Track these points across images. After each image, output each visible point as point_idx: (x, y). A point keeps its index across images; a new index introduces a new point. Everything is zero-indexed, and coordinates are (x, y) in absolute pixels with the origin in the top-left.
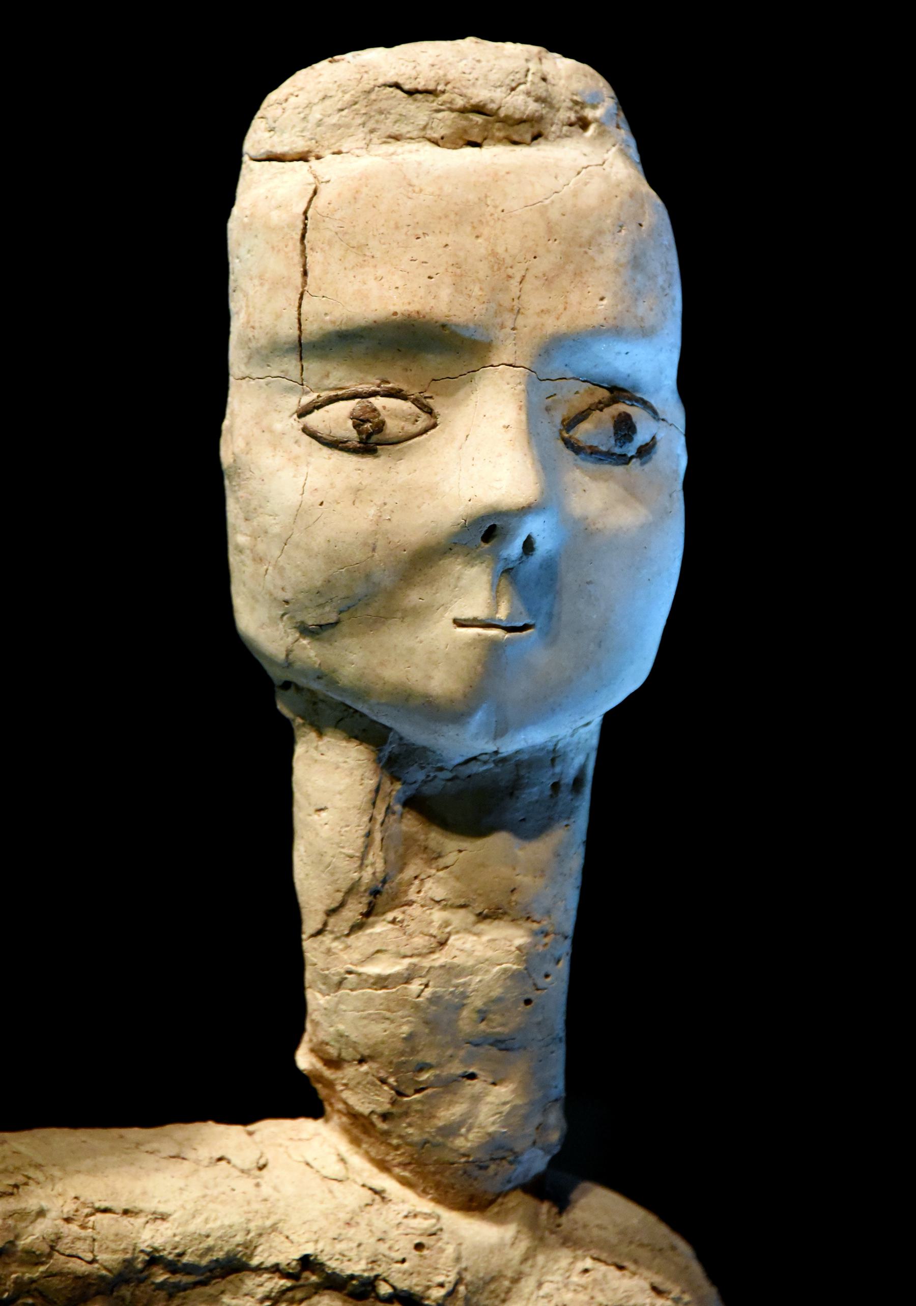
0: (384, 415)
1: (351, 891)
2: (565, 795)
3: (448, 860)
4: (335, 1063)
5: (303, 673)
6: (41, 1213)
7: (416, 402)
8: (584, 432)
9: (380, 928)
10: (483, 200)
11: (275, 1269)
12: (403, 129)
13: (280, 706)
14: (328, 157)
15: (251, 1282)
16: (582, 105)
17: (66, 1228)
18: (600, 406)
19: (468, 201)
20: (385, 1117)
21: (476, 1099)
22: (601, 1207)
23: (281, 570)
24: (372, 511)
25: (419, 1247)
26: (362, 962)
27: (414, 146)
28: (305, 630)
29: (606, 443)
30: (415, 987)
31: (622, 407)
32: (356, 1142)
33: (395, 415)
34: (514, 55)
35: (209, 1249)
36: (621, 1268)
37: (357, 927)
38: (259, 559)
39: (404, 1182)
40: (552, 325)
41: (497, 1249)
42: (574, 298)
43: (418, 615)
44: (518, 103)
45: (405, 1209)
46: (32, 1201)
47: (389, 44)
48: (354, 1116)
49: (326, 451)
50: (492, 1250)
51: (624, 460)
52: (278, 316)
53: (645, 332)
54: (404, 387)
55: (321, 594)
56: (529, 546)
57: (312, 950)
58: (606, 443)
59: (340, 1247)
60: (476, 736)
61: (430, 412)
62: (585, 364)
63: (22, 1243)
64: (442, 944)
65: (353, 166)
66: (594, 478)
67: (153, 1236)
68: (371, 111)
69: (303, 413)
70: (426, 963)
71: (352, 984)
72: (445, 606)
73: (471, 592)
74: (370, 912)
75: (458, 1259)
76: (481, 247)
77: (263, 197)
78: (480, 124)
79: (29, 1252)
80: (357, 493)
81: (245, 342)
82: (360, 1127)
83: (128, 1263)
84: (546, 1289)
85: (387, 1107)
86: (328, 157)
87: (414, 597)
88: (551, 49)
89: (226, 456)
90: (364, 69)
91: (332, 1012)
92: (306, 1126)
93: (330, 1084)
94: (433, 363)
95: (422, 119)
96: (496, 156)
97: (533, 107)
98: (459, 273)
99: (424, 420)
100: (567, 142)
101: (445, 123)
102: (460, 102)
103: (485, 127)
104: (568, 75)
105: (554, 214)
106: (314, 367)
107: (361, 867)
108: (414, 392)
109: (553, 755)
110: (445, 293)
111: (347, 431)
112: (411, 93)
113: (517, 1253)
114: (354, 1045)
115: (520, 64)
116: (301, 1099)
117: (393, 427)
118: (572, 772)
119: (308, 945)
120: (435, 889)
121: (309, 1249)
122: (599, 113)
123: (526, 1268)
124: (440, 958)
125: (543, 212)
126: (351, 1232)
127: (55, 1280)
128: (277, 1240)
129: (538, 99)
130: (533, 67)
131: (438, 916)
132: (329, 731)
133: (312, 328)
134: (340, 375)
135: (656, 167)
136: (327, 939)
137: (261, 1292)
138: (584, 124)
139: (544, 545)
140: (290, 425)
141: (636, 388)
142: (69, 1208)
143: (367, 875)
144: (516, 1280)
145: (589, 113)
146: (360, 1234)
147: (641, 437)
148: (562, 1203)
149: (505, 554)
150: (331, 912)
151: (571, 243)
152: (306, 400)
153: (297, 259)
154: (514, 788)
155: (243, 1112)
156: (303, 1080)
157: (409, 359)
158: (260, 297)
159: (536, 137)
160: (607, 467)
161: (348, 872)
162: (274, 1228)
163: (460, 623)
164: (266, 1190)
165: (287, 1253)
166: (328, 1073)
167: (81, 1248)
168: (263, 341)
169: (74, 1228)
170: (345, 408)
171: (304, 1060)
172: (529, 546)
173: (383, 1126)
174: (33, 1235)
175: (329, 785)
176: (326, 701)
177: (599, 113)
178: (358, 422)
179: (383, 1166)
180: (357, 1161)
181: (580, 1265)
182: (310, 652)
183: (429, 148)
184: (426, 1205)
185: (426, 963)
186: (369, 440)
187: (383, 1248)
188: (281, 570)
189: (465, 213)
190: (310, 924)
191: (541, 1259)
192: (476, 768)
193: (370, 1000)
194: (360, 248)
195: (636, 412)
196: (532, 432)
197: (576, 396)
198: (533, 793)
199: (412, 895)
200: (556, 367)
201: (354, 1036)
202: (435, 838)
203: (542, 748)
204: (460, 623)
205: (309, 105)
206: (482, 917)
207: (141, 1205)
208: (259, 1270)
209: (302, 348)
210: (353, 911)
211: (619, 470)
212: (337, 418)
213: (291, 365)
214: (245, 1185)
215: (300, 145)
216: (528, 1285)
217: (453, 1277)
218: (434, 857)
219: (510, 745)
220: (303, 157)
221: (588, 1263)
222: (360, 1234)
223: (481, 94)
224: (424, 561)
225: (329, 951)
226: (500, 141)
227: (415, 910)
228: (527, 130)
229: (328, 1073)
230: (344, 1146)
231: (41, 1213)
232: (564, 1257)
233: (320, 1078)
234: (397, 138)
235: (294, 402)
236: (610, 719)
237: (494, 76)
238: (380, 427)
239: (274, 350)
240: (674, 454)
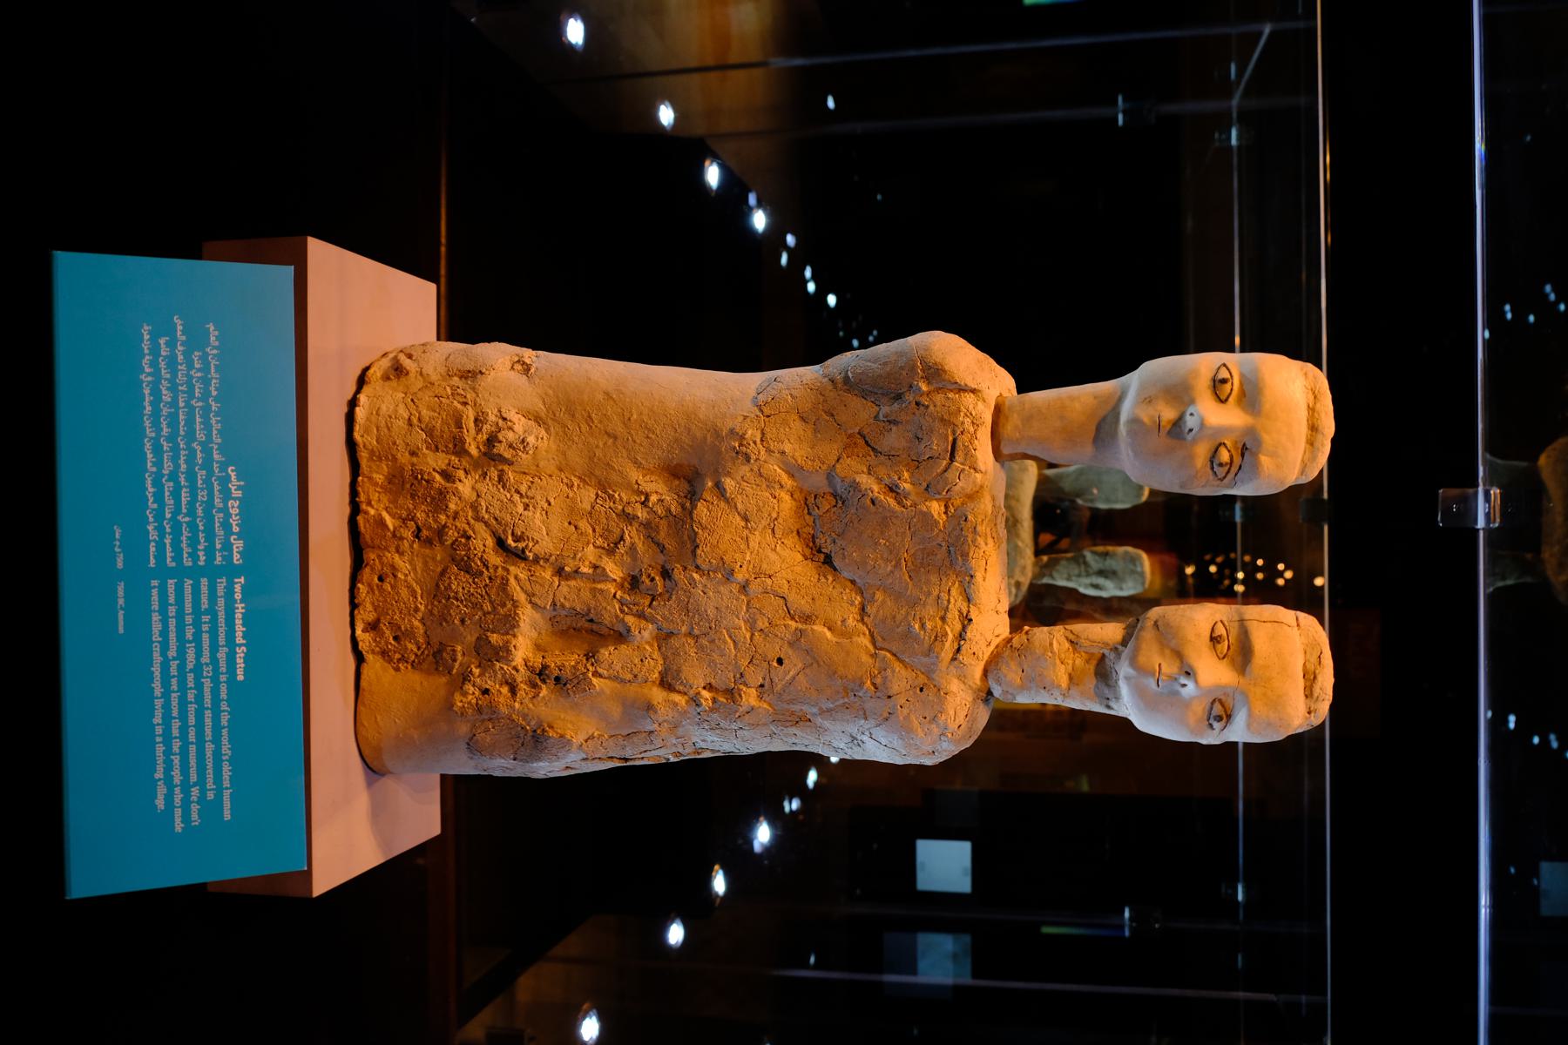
9: (1067, 645)
19: (955, 957)
29: (1214, 713)
43: (1162, 653)
44: (1317, 691)
46: (990, 541)
58: (1214, 713)
67: (979, 576)
68: (1311, 646)
78: (1310, 678)
80: (1198, 635)
82: (1009, 641)
87: (1167, 652)
94: (1239, 659)
96: (1301, 683)
101: (1310, 667)
116: (1015, 629)
117: (1219, 647)
120: (1078, 661)
134: (1234, 632)
139: (1184, 691)
147: (1216, 725)
151: (1276, 703)
154: (1108, 686)
157: (1242, 654)
165: (972, 615)
182: (1150, 624)
186: (1215, 640)
196: (1218, 687)
197: (1229, 702)
198: (1106, 691)
210: (1071, 637)
212: (1220, 630)
223: (1319, 678)
224: (1179, 655)
228: (1309, 693)
232: (970, 699)
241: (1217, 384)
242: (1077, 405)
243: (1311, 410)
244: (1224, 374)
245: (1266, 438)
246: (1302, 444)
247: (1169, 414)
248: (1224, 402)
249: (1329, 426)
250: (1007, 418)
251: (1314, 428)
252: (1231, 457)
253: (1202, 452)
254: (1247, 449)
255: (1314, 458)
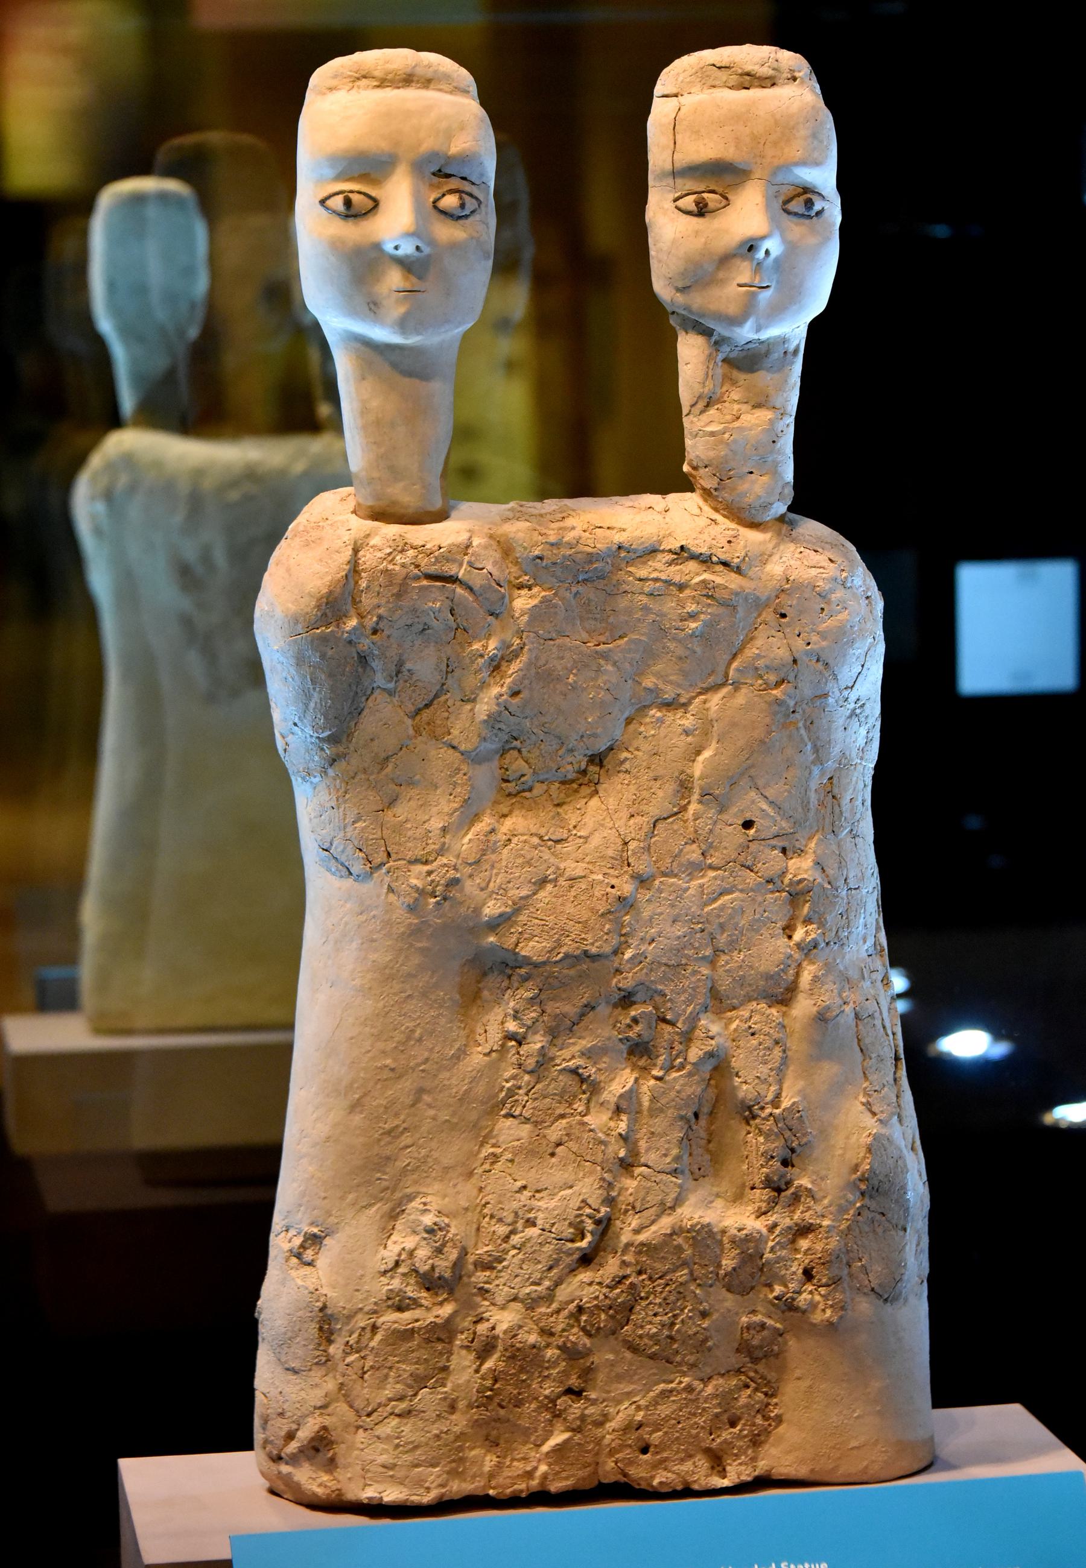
0: (708, 201)
1: (699, 397)
2: (789, 356)
3: (741, 383)
4: (695, 468)
5: (679, 307)
6: (573, 528)
7: (721, 195)
8: (792, 206)
9: (712, 411)
10: (748, 111)
11: (670, 551)
12: (717, 83)
13: (671, 322)
14: (686, 95)
15: (660, 556)
16: (794, 71)
17: (584, 534)
18: (798, 195)
20: (716, 490)
21: (753, 482)
22: (812, 528)
23: (667, 265)
24: (703, 240)
25: (729, 542)
26: (705, 426)
27: (721, 90)
28: (678, 290)
29: (801, 210)
30: (726, 436)
31: (808, 196)
32: (706, 500)
33: (712, 200)
34: (766, 51)
35: (643, 543)
36: (816, 551)
37: (702, 412)
38: (660, 261)
39: (724, 516)
40: (776, 162)
41: (764, 542)
42: (786, 150)
43: (722, 282)
44: (766, 71)
45: (724, 527)
46: (569, 522)
47: (713, 48)
48: (704, 489)
49: (684, 216)
50: (760, 543)
51: (810, 217)
52: (664, 161)
53: (817, 164)
54: (716, 188)
55: (683, 274)
56: (767, 252)
57: (686, 422)
58: (801, 210)
59: (696, 542)
60: (748, 332)
61: (727, 199)
62: (790, 179)
63: (565, 540)
64: (738, 418)
65: (697, 99)
66: (797, 224)
67: (618, 538)
69: (675, 200)
70: (731, 426)
71: (701, 436)
72: (734, 279)
73: (743, 273)
74: (708, 405)
75: (745, 547)
76: (748, 130)
77: (660, 112)
78: (749, 80)
79: (568, 543)
80: (697, 233)
81: (653, 172)
82: (707, 494)
83: (609, 549)
84: (784, 559)
85: (716, 486)
86: (686, 95)
88: (782, 47)
89: (647, 220)
90: (701, 59)
91: (694, 446)
92: (689, 494)
93: (694, 477)
94: (729, 179)
95: (724, 78)
96: (755, 93)
97: (771, 72)
98: (738, 141)
99: (724, 202)
100: (786, 87)
101: (734, 80)
102: (740, 71)
103: (750, 82)
104: (789, 59)
105: (778, 116)
106: (679, 181)
107: (704, 387)
108: (720, 190)
109: (784, 340)
110: (732, 150)
111: (693, 207)
112: (719, 68)
113: (770, 546)
114: (702, 460)
115: (766, 55)
116: (685, 485)
117: (711, 205)
118: (792, 347)
119: (685, 420)
121: (683, 543)
122: (801, 74)
123: (775, 551)
124: (736, 424)
125: (773, 115)
126: (701, 536)
127: (579, 556)
128: (671, 539)
129: (774, 69)
130: (772, 56)
131: (736, 407)
132: (690, 331)
133: (677, 165)
134: (690, 185)
135: (830, 98)
136: (691, 417)
137: (664, 561)
138: (795, 79)
140: (669, 205)
141: (815, 187)
142: (585, 527)
143: (706, 390)
144: (770, 556)
145: (797, 74)
146: (705, 537)
147: (817, 207)
148: (792, 524)
149: (757, 256)
150: (692, 406)
152: (677, 195)
153: (672, 137)
154: (767, 354)
155: (663, 490)
156: (685, 476)
158: (658, 156)
159: (773, 85)
160: (802, 220)
161: (698, 389)
162: (670, 534)
163: (740, 285)
164: (667, 520)
165: (675, 545)
166: (693, 472)
167: (590, 542)
168: (659, 172)
169: (587, 534)
170: (692, 198)
171: (686, 468)
172: (767, 252)
173: (716, 493)
174: (569, 537)
175: (690, 352)
176: (689, 318)
177: (801, 74)
178: (697, 203)
179: (716, 510)
180: (706, 508)
181: (799, 550)
183: (727, 90)
184: (733, 525)
185: (731, 426)
186: (701, 211)
187: (714, 542)
188: (667, 265)
189: (740, 117)
190: (685, 412)
191: (782, 547)
192: (750, 346)
193: (708, 441)
194: (697, 132)
195: (814, 197)
196: (768, 206)
197: (787, 191)
198: (776, 355)
199: (725, 398)
200: (780, 178)
201: (702, 457)
202: (735, 374)
203: (779, 337)
204: (740, 285)
205: (678, 74)
206: (754, 407)
207: (614, 525)
208: (663, 551)
209: (675, 174)
210: (701, 405)
211: (807, 221)
212: (689, 202)
213: (670, 181)
214: (659, 517)
215: (674, 91)
216: (775, 558)
217: (743, 554)
218: (734, 383)
219: (764, 335)
220: (676, 96)
221: (802, 549)
222: (705, 537)
223: (749, 68)
224: (726, 259)
225: (692, 422)
226: (757, 87)
227: (727, 404)
228: (769, 82)
229: (693, 472)
230: (701, 503)
231: (573, 528)
233: (691, 475)
234: (714, 87)
235: (672, 196)
236: (814, 326)
237: (755, 60)
238: (706, 205)
239: (663, 175)
240: (835, 214)
241: (351, 212)
242: (375, 404)
243: (383, 83)
244: (338, 203)
245: (428, 145)
246: (430, 95)
247: (394, 279)
248: (376, 203)
249: (401, 58)
250: (394, 503)
251: (408, 80)
252: (451, 192)
253: (446, 232)
254: (441, 171)
255: (447, 77)
